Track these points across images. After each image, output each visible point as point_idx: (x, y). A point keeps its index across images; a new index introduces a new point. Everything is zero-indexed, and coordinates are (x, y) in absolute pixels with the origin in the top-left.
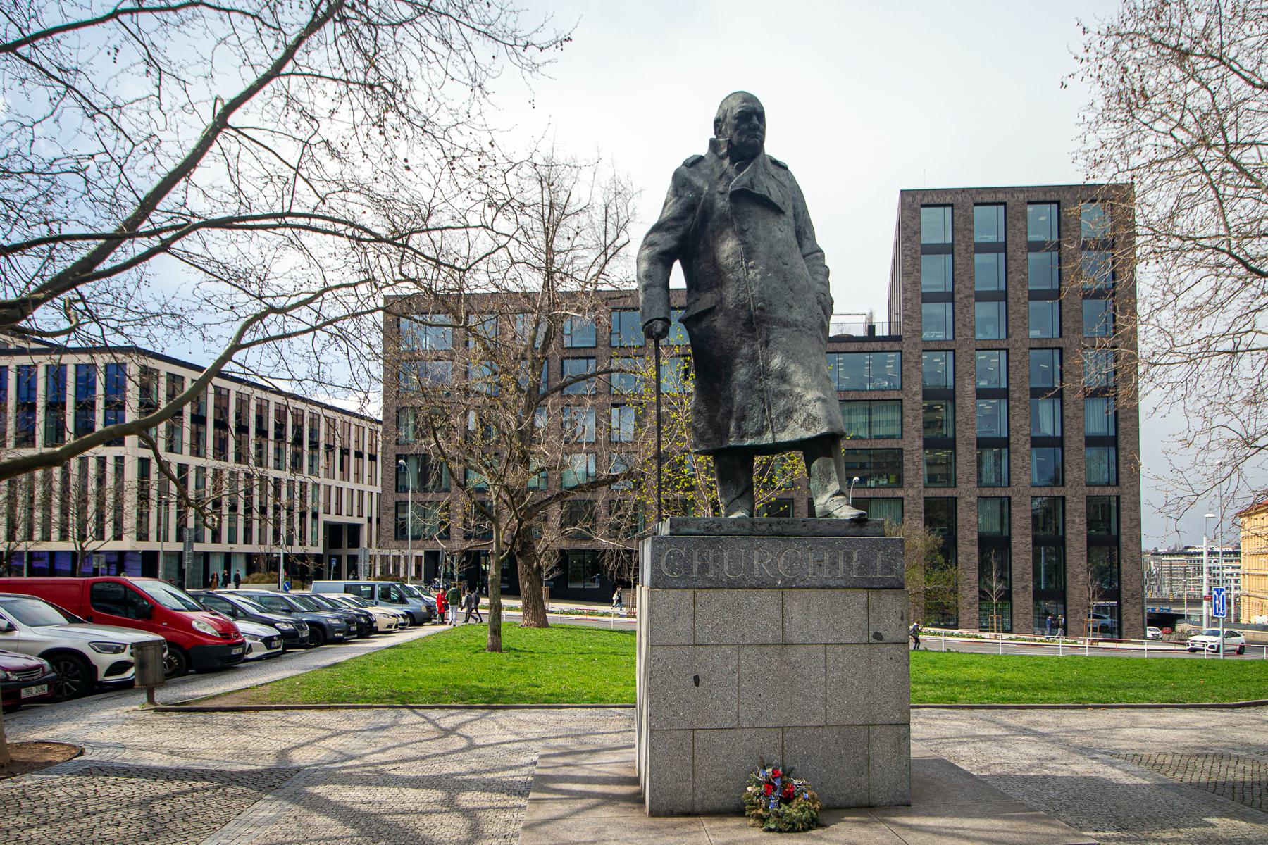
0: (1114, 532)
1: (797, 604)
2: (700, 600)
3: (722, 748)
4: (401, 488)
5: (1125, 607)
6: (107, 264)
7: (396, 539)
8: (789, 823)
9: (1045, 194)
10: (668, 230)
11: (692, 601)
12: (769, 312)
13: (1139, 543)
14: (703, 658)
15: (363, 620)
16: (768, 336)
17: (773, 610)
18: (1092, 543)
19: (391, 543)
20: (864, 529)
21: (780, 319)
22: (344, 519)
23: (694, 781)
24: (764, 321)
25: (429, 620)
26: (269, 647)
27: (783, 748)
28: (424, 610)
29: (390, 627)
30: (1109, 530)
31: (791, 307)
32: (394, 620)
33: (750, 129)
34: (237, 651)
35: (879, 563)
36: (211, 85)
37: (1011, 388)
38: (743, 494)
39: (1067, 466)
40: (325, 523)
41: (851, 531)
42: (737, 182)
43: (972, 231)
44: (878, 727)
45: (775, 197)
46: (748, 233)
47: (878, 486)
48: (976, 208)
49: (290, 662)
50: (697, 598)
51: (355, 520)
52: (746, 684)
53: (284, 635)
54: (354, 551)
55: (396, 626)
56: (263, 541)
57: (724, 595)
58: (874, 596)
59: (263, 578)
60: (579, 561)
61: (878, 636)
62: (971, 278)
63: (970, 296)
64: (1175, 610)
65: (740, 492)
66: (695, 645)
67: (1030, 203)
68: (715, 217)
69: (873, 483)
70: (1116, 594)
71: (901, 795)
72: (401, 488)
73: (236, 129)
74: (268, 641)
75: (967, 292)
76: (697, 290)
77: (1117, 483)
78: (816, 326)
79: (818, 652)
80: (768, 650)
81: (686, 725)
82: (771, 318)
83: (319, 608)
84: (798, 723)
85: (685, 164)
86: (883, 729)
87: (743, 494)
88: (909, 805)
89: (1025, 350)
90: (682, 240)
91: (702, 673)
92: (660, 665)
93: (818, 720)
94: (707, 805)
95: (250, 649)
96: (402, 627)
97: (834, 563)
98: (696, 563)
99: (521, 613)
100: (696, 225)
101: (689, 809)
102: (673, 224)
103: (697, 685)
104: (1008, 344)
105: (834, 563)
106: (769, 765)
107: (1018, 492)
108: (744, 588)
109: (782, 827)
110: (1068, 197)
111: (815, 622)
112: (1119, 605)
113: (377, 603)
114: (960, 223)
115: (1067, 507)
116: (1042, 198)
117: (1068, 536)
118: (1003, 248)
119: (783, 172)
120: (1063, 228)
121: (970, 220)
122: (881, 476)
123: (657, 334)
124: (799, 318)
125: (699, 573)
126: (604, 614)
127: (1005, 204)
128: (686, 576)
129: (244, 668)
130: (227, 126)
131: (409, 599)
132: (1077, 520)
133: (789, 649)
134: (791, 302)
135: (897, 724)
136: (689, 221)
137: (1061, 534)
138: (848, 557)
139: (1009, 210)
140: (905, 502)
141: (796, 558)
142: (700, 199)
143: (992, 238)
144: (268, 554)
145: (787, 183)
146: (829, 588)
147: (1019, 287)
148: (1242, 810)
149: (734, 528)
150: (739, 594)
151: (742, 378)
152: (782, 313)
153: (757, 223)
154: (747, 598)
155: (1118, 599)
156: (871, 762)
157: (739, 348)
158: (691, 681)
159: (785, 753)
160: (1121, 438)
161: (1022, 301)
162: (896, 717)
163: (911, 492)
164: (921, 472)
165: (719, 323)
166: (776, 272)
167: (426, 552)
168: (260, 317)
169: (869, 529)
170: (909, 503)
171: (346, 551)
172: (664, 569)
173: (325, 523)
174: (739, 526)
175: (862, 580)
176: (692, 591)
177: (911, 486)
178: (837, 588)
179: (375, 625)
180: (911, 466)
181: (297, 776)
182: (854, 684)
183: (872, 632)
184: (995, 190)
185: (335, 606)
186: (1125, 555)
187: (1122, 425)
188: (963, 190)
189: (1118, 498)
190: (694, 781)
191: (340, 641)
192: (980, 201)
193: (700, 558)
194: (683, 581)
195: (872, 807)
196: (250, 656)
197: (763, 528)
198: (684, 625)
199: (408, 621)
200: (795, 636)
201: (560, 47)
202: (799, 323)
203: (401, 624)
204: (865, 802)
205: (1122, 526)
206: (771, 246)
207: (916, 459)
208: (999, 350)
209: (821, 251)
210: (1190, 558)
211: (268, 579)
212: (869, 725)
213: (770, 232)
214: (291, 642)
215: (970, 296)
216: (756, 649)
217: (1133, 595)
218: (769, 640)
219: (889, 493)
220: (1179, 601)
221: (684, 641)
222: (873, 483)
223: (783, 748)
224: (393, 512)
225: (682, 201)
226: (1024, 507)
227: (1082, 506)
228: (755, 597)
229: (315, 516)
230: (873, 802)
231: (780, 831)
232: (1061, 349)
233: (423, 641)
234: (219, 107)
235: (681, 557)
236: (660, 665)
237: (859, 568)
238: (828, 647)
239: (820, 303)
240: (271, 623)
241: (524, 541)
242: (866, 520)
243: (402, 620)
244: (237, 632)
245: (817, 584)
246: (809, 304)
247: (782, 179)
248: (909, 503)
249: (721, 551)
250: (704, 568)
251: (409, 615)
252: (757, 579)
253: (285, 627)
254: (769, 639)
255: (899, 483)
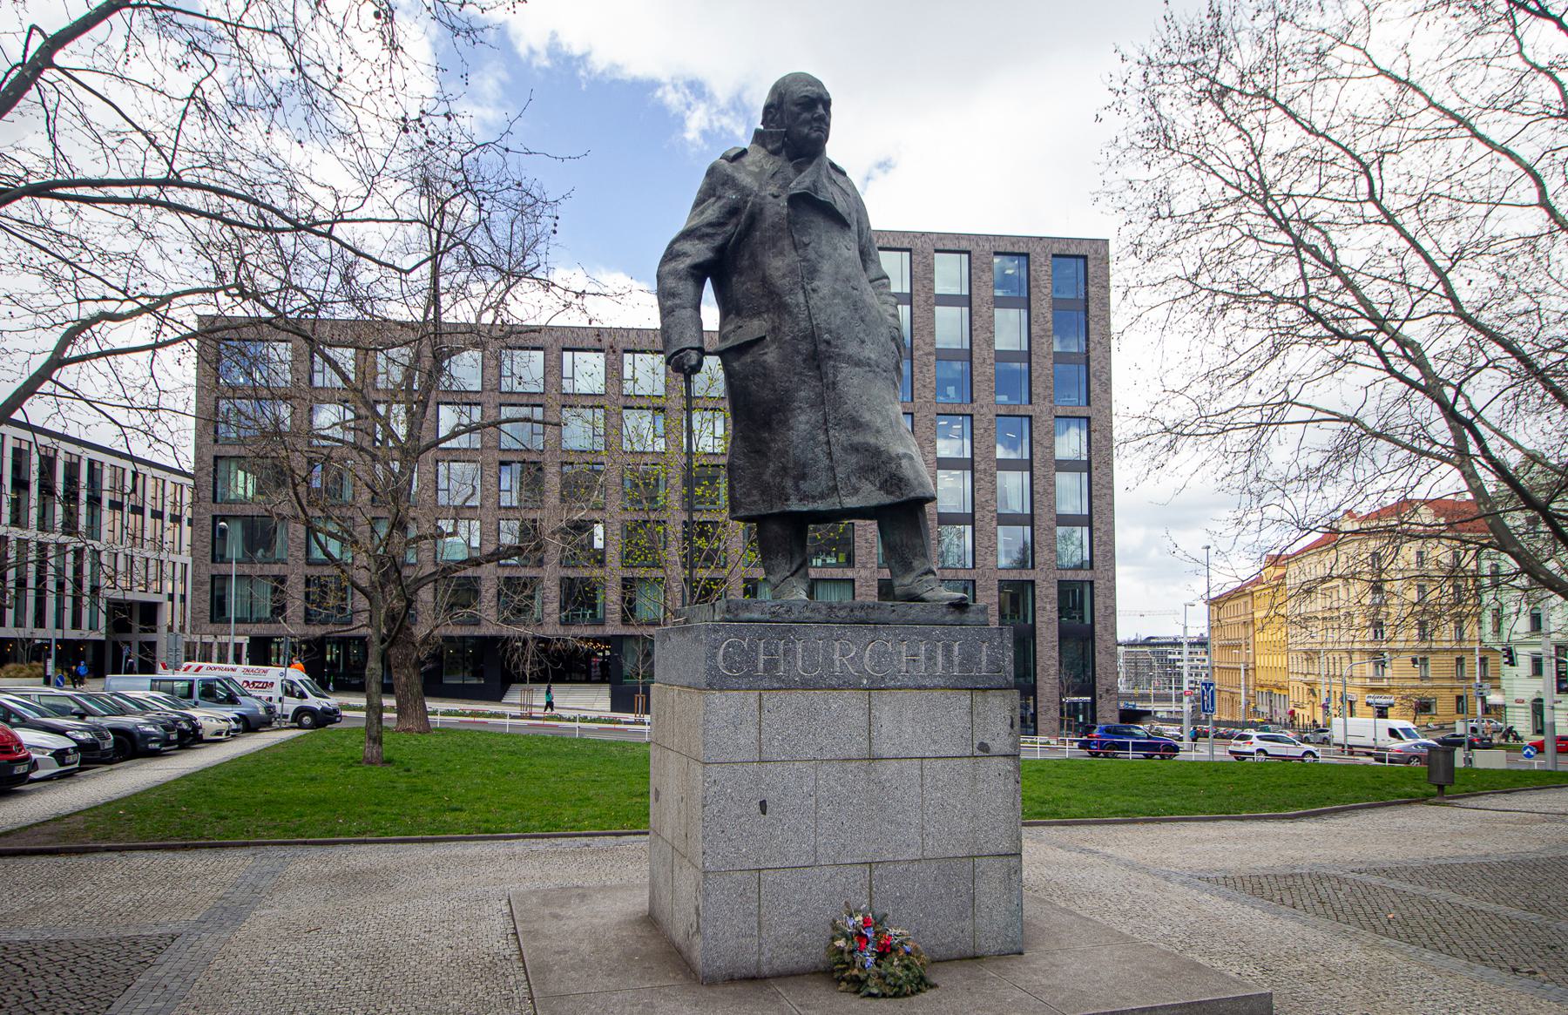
0: (1088, 621)
1: (887, 708)
2: (768, 705)
3: (795, 892)
4: (217, 557)
5: (1099, 703)
6: (60, 191)
7: (212, 621)
8: (895, 986)
9: (1013, 244)
10: (702, 237)
11: (756, 705)
12: (836, 346)
13: (1114, 633)
14: (771, 778)
15: (185, 726)
16: (835, 376)
17: (857, 716)
18: (1064, 636)
19: (204, 626)
20: (964, 616)
21: (850, 356)
22: (136, 596)
23: (760, 936)
24: (830, 357)
25: (269, 724)
26: (62, 764)
27: (871, 889)
28: (262, 712)
29: (219, 733)
30: (1082, 618)
31: (863, 342)
32: (224, 725)
33: (815, 120)
34: (21, 769)
35: (984, 658)
36: (22, 12)
37: (976, 458)
38: (796, 571)
39: (1036, 546)
40: (110, 602)
41: (949, 618)
42: (799, 183)
43: (932, 281)
44: (985, 859)
45: (841, 206)
46: (809, 248)
47: (825, 565)
48: (936, 255)
49: (93, 782)
50: (763, 702)
51: (150, 597)
52: (826, 810)
53: (81, 746)
54: (149, 637)
55: (227, 734)
56: (94, 626)
57: (798, 697)
58: (978, 697)
59: (21, 671)
60: (457, 651)
61: (984, 747)
62: (932, 334)
63: (930, 354)
64: (1140, 706)
65: (794, 568)
66: (761, 761)
67: (996, 254)
68: (766, 225)
69: (819, 562)
70: (1090, 689)
71: (1013, 941)
72: (217, 557)
73: (62, 70)
74: (60, 755)
75: (928, 349)
76: (738, 314)
77: (1091, 567)
78: (891, 368)
79: (913, 768)
80: (851, 766)
81: (750, 864)
82: (839, 355)
83: (123, 711)
84: (890, 857)
85: (724, 157)
86: (991, 860)
87: (796, 571)
88: (1021, 953)
89: (991, 416)
90: (720, 250)
91: (771, 796)
92: (715, 789)
93: (914, 853)
94: (777, 964)
95: (34, 766)
96: (233, 734)
97: (931, 658)
98: (762, 657)
99: (395, 715)
100: (739, 234)
101: (754, 972)
102: (709, 230)
103: (764, 813)
104: (973, 409)
105: (931, 658)
106: (858, 911)
107: (984, 574)
108: (821, 689)
109: (887, 990)
110: (1038, 250)
111: (910, 730)
112: (1094, 702)
113: (196, 703)
114: (918, 270)
115: (1037, 592)
116: (1010, 249)
117: (1038, 625)
118: (967, 301)
119: (840, 179)
120: (1032, 284)
121: (930, 269)
122: (828, 554)
123: (690, 367)
124: (872, 356)
125: (765, 670)
126: (496, 715)
127: (969, 253)
128: (748, 674)
129: (30, 792)
130: (53, 66)
131: (241, 699)
132: (1048, 607)
133: (877, 765)
134: (862, 335)
135: (1006, 855)
136: (729, 228)
137: (1030, 622)
138: (948, 650)
139: (973, 260)
140: (857, 584)
141: (885, 652)
142: (746, 202)
143: (955, 290)
144: (29, 640)
145: (849, 191)
146: (925, 688)
147: (984, 346)
148: (1382, 942)
149: (807, 614)
150: (817, 696)
151: (802, 427)
152: (852, 348)
153: (820, 237)
154: (826, 702)
155: (1092, 693)
156: (977, 902)
157: (798, 390)
158: (756, 808)
159: (874, 895)
160: (1095, 518)
161: (988, 362)
162: (1005, 846)
163: (863, 573)
164: (875, 551)
165: (771, 356)
166: (845, 298)
167: (251, 638)
168: (85, 325)
169: (970, 616)
170: (861, 586)
171: (137, 636)
172: (721, 665)
173: (110, 602)
174: (813, 610)
175: (964, 678)
176: (757, 692)
177: (864, 567)
178: (935, 688)
179: (200, 732)
180: (863, 543)
181: (174, 946)
182: (955, 807)
183: (976, 743)
184: (958, 237)
185: (142, 707)
186: (1099, 645)
187: (1096, 502)
188: (923, 234)
189: (1092, 583)
190: (760, 936)
191: (156, 754)
192: (942, 247)
193: (767, 652)
194: (746, 680)
195: (975, 958)
196: (34, 775)
197: (843, 613)
198: (748, 735)
199: (240, 726)
200: (885, 749)
201: (512, 9)
202: (872, 363)
203: (234, 731)
204: (970, 952)
205: (1096, 614)
206: (838, 267)
207: (869, 536)
208: (963, 415)
209: (887, 278)
210: (1153, 649)
211: (28, 671)
212: (973, 857)
213: (836, 249)
214: (91, 756)
215: (930, 354)
216: (837, 765)
217: (1107, 691)
218: (854, 754)
219: (838, 573)
220: (1145, 698)
221: (746, 757)
222: (819, 562)
223: (871, 889)
224: (208, 587)
225: (721, 203)
226: (989, 592)
227: (1054, 591)
228: (838, 701)
229: (95, 589)
230: (979, 953)
231: (884, 996)
232: (1030, 417)
233: (257, 756)
234: (37, 42)
235: (743, 650)
236: (715, 789)
237: (961, 664)
238: (925, 762)
239: (893, 339)
240: (61, 732)
241: (399, 623)
242: (967, 605)
243: (234, 725)
244: (20, 744)
245: (911, 684)
246: (883, 339)
247: (844, 186)
248: (861, 586)
249: (793, 642)
250: (771, 665)
251: (242, 719)
252: (837, 677)
253: (81, 736)
254: (854, 753)
255: (850, 562)
